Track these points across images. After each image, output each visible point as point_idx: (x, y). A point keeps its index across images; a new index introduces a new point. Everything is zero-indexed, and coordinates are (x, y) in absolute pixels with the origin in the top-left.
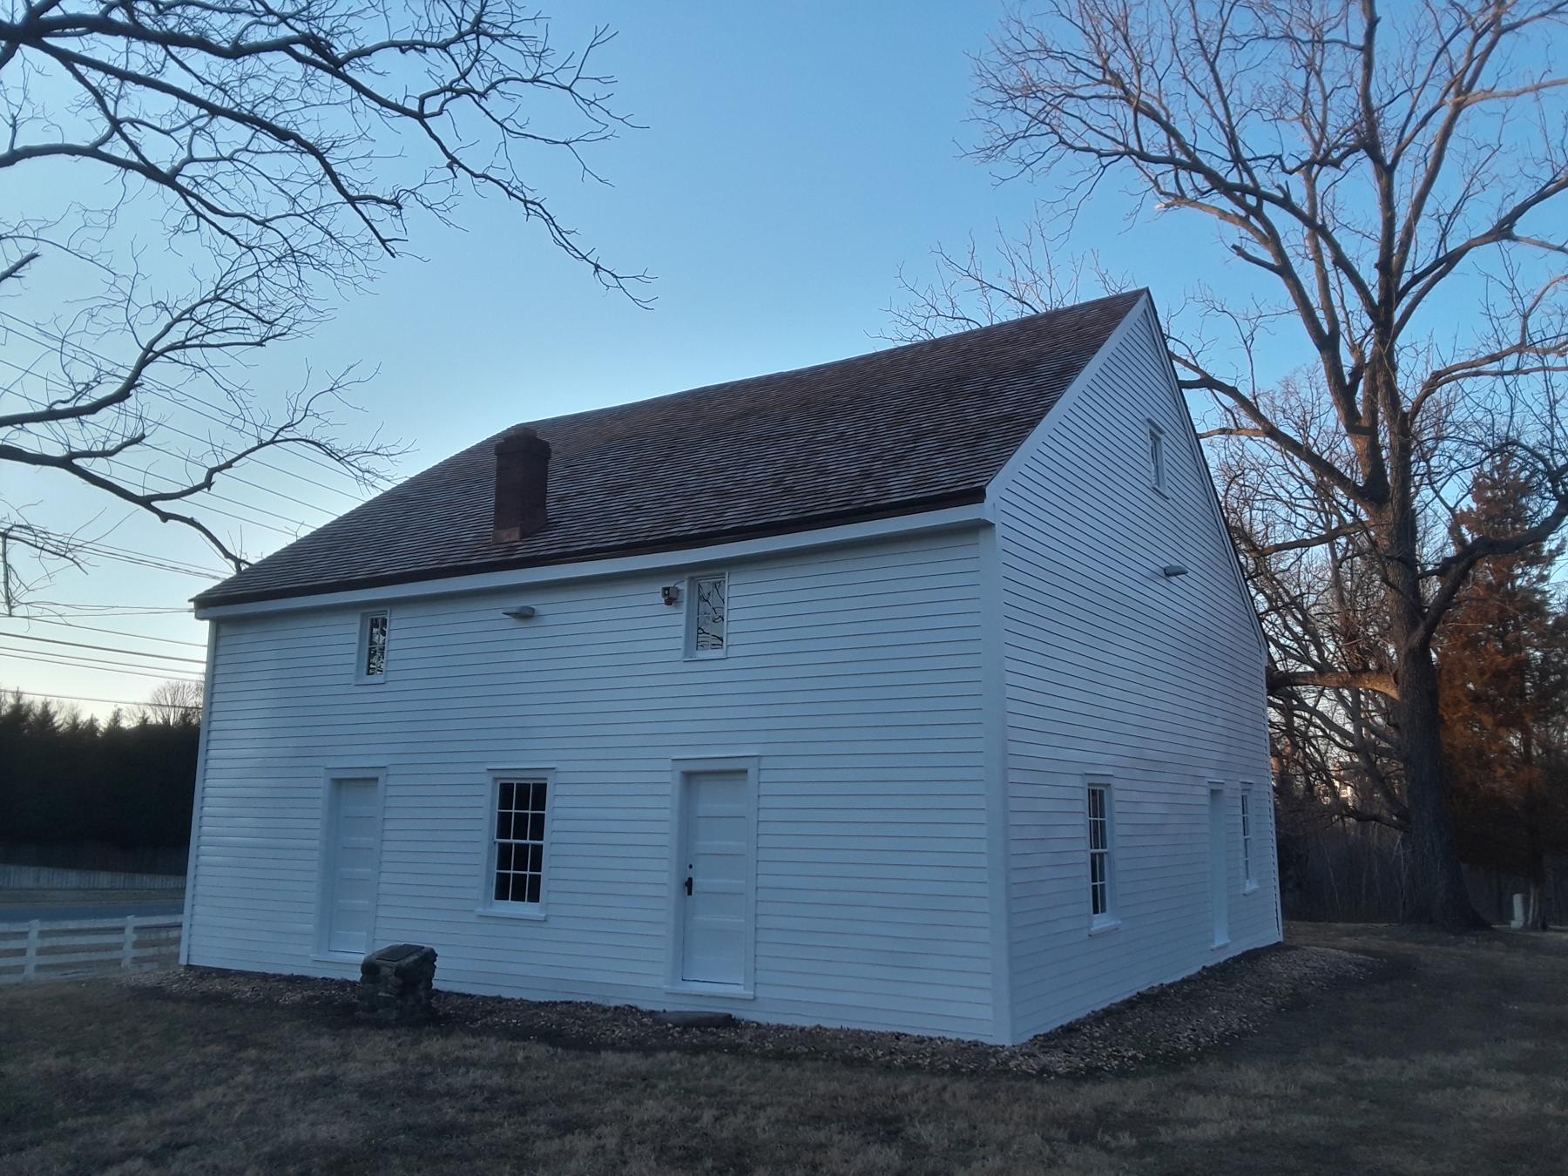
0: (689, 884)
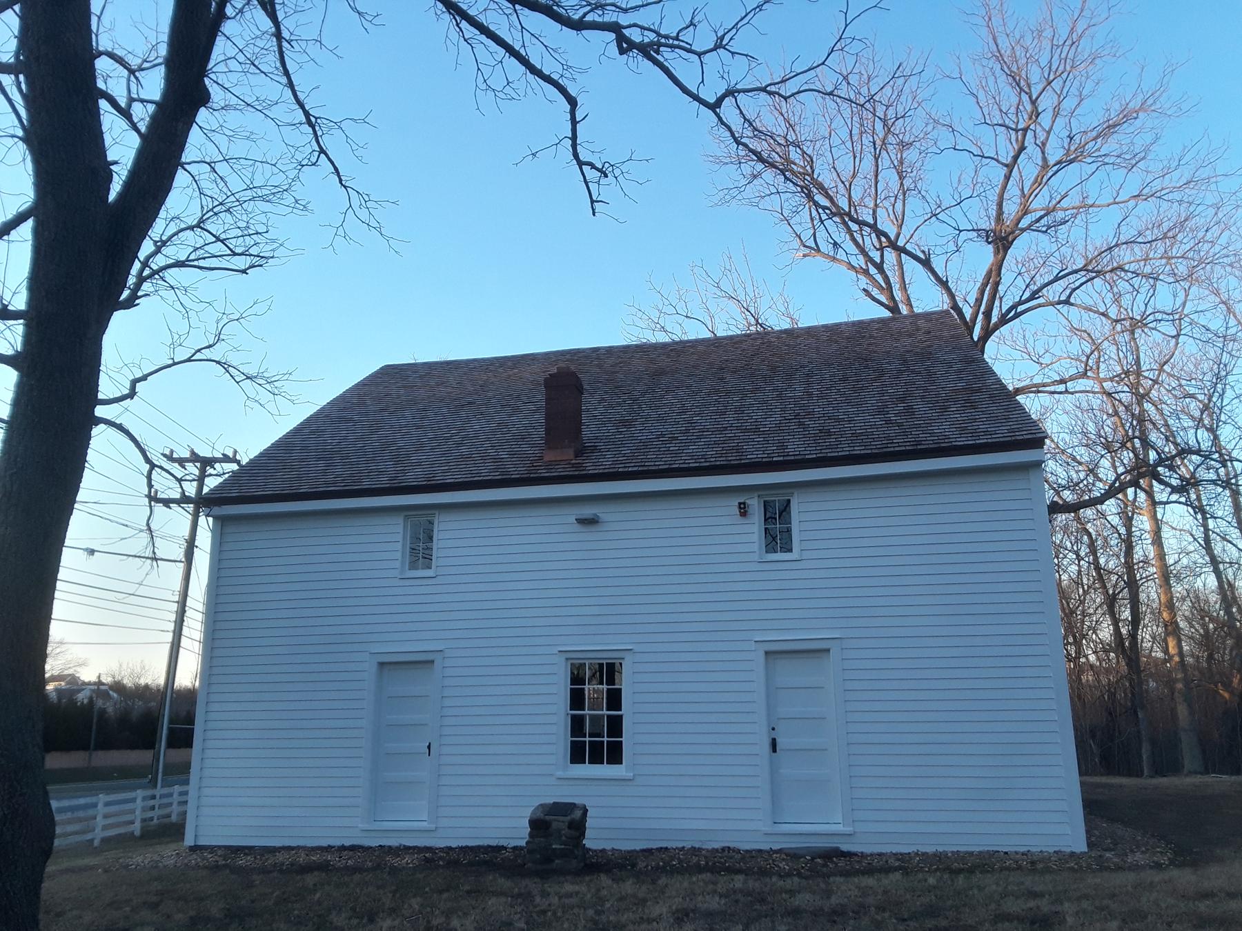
0: (774, 745)
